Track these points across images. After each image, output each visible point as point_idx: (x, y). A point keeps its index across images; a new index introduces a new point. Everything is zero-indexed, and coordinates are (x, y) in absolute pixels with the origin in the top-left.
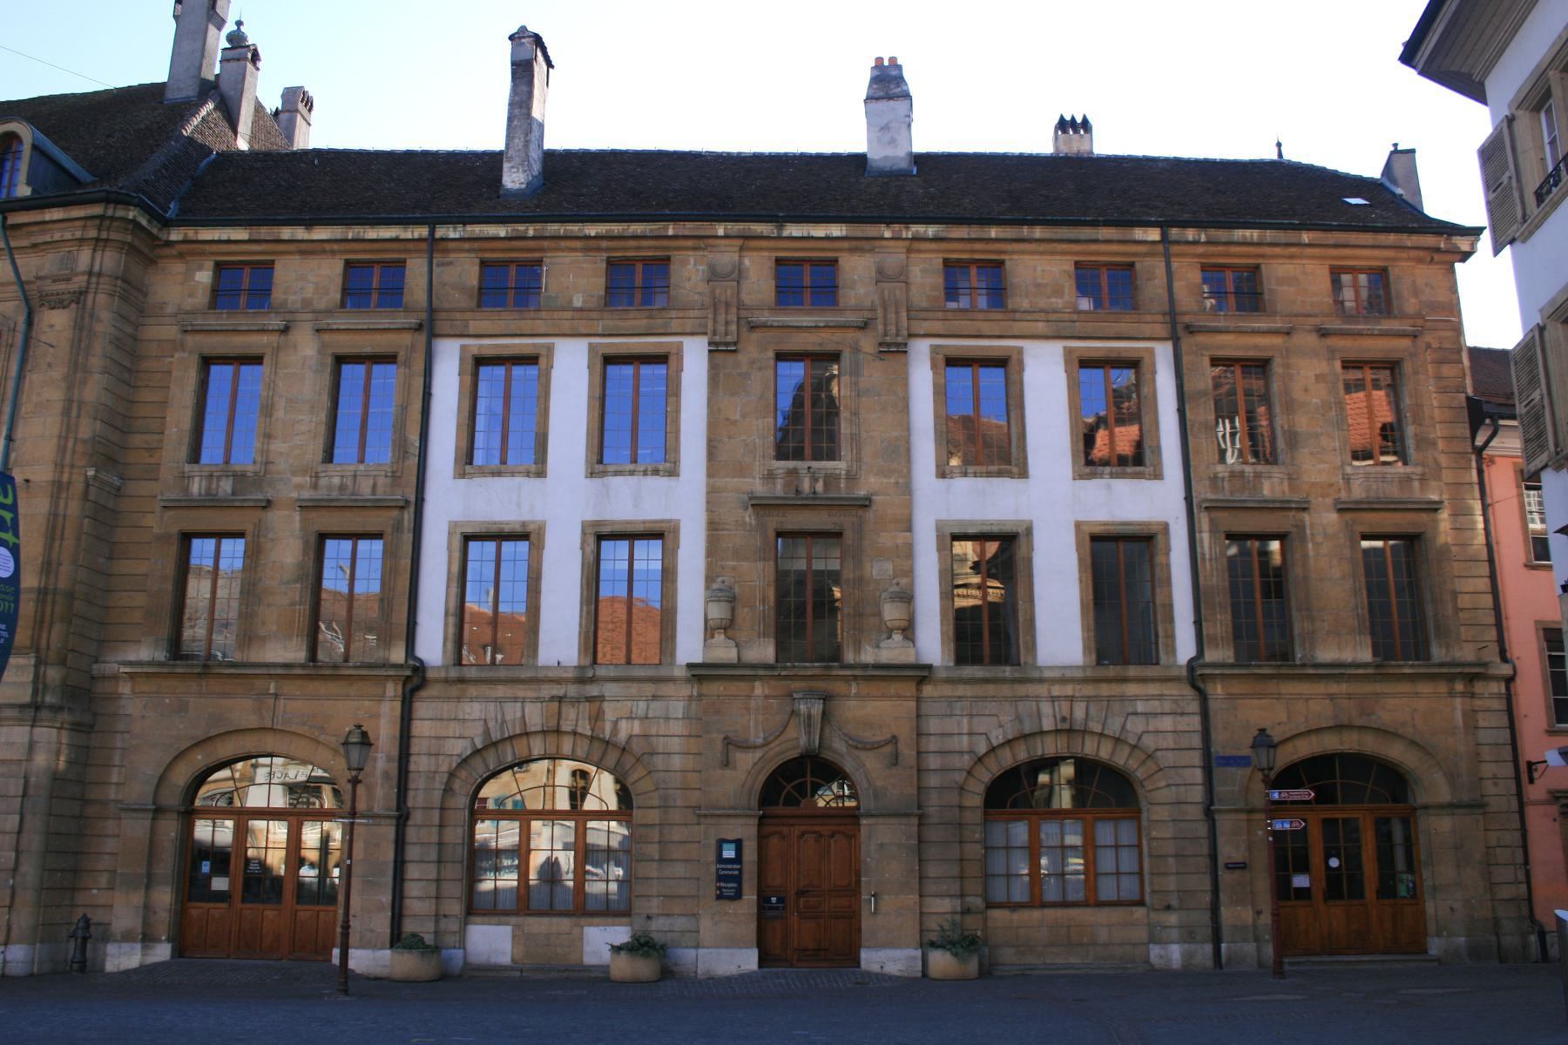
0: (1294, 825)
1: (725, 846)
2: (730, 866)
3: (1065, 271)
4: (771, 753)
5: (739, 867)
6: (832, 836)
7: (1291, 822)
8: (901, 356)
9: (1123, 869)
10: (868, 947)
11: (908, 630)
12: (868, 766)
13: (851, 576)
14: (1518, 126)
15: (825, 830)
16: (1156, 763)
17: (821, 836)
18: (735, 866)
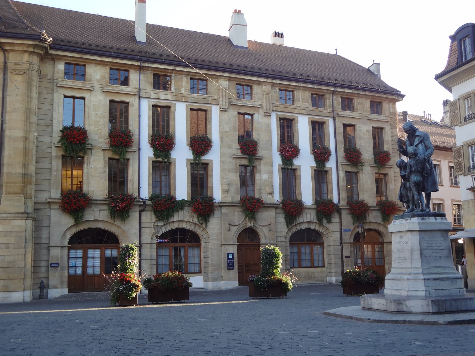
0: (165, 241)
2: (231, 260)
3: (309, 96)
7: (165, 240)
8: (269, 117)
9: (92, 260)
11: (272, 194)
14: (460, 101)
16: (329, 231)
18: (232, 260)
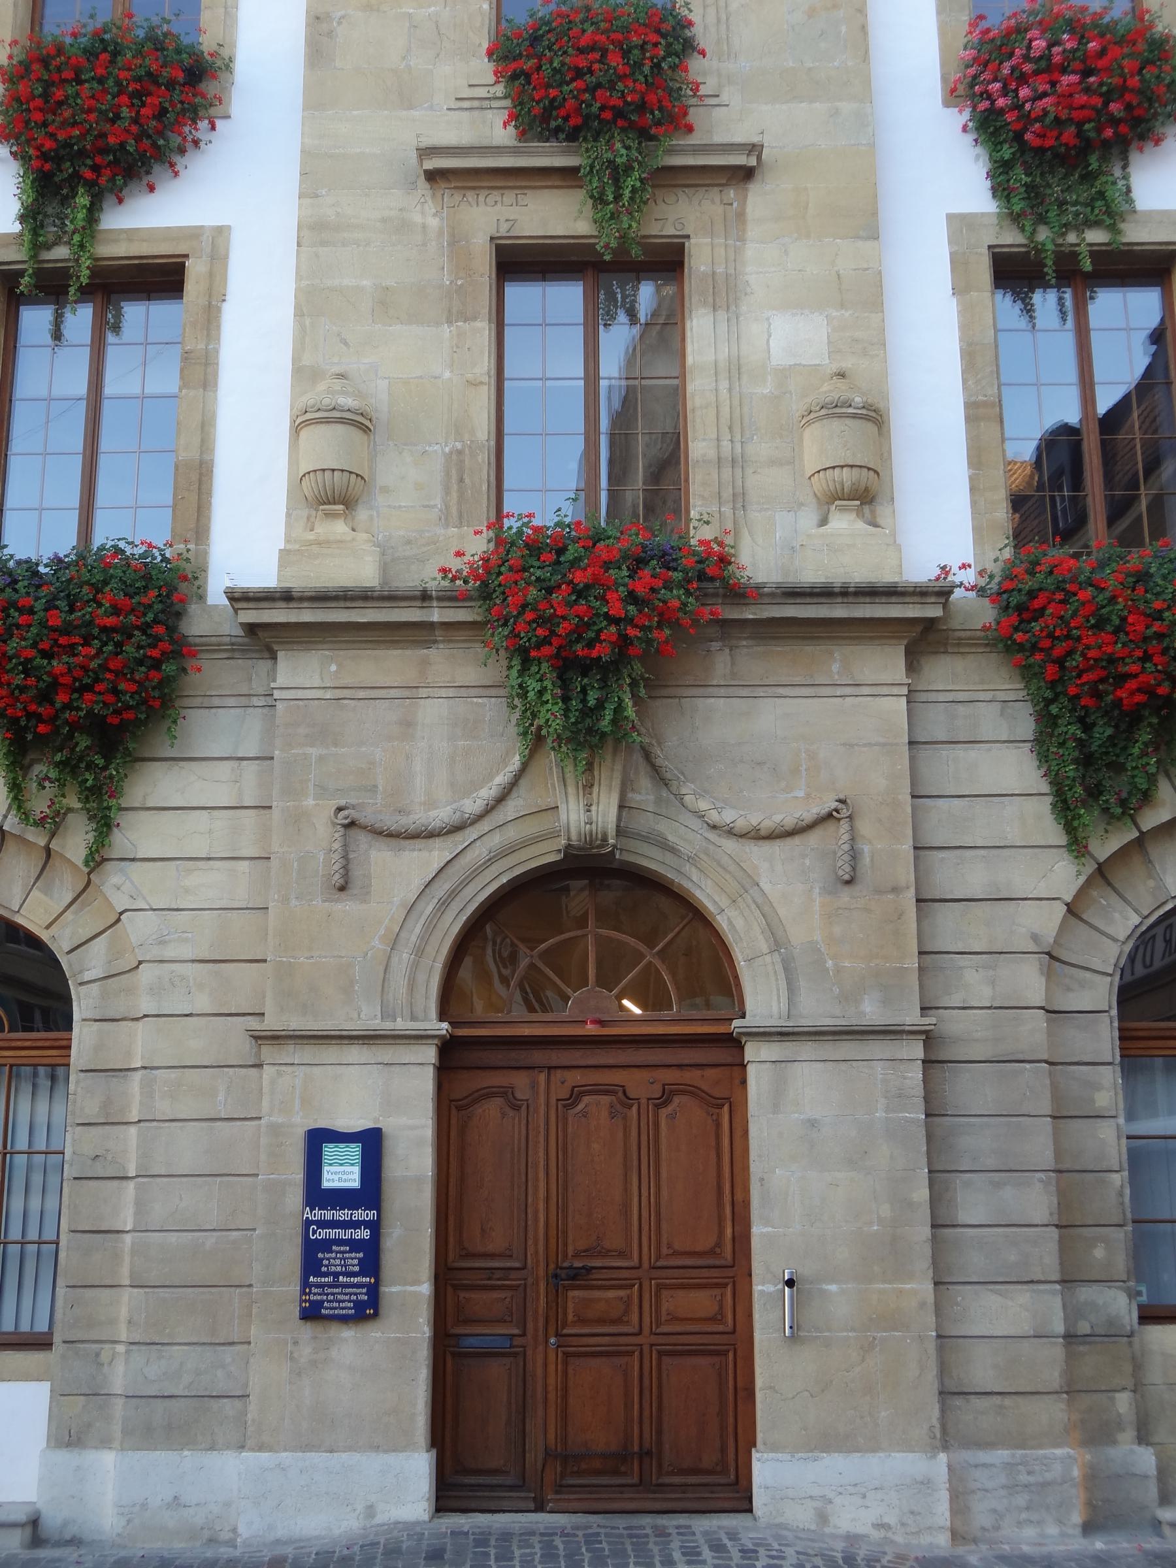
1: (330, 1151)
2: (343, 1215)
4: (480, 852)
5: (371, 1215)
6: (664, 1099)
10: (774, 1448)
12: (766, 886)
13: (709, 357)
15: (640, 1084)
17: (627, 1100)
18: (360, 1215)
